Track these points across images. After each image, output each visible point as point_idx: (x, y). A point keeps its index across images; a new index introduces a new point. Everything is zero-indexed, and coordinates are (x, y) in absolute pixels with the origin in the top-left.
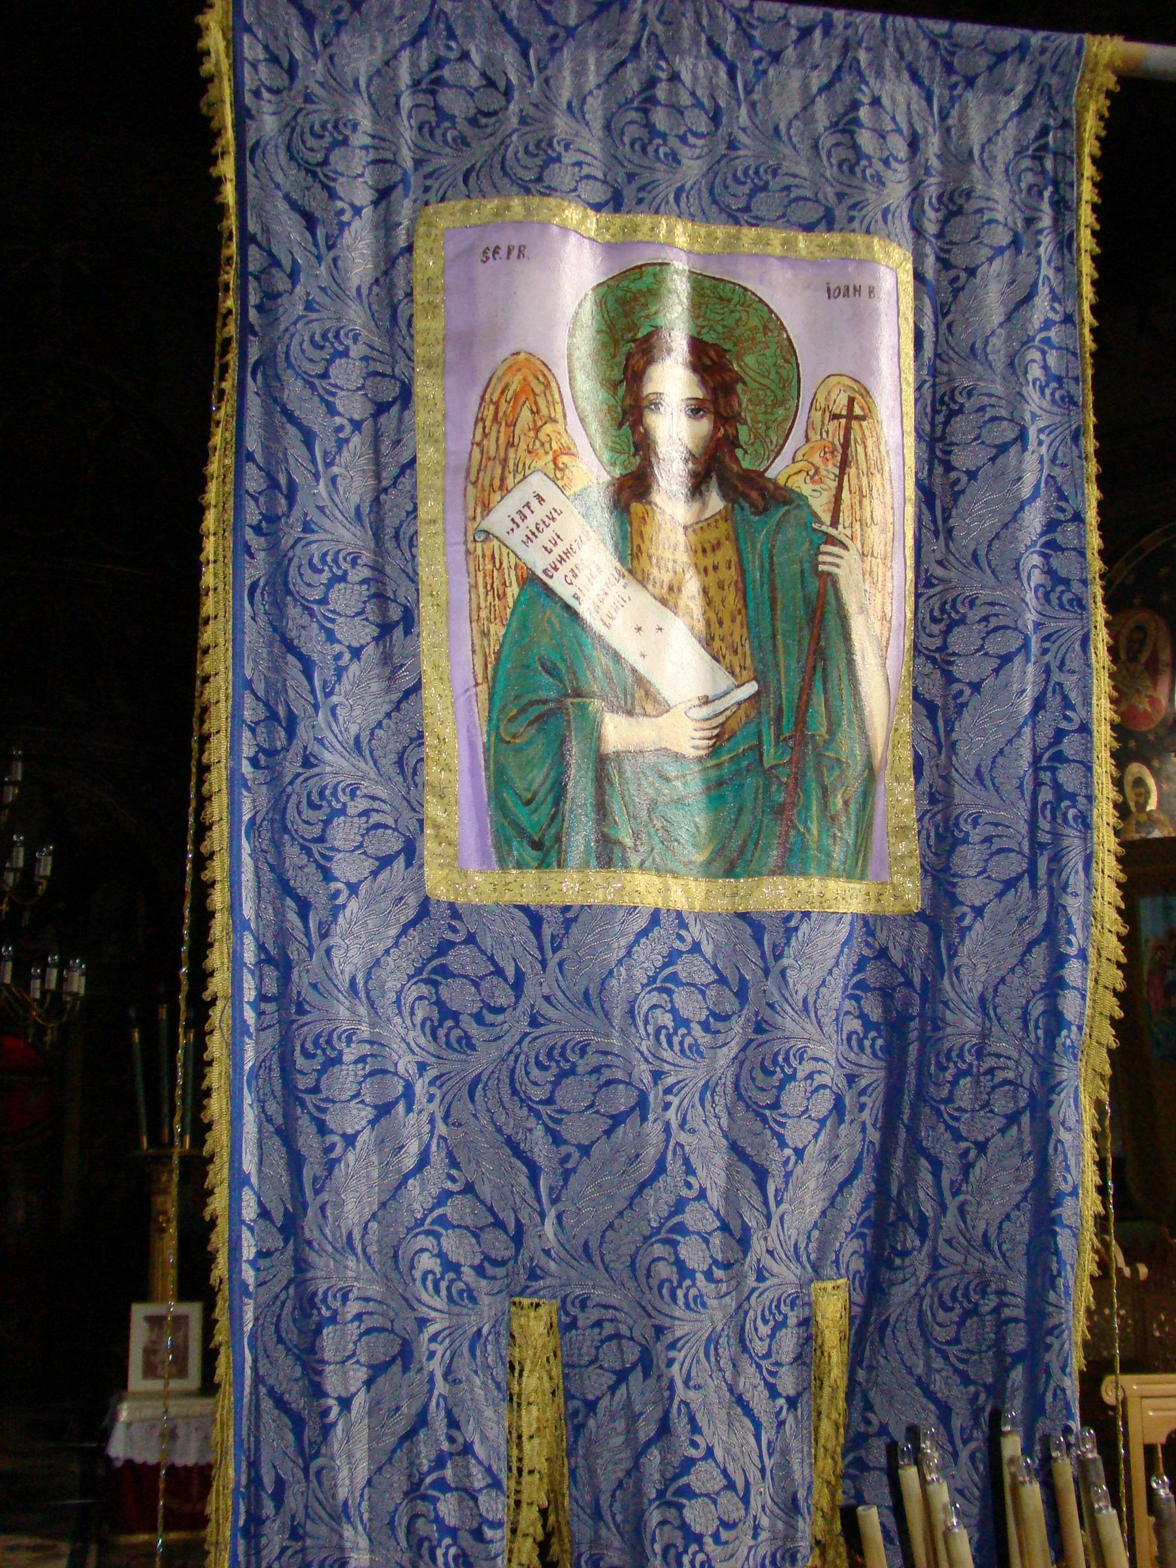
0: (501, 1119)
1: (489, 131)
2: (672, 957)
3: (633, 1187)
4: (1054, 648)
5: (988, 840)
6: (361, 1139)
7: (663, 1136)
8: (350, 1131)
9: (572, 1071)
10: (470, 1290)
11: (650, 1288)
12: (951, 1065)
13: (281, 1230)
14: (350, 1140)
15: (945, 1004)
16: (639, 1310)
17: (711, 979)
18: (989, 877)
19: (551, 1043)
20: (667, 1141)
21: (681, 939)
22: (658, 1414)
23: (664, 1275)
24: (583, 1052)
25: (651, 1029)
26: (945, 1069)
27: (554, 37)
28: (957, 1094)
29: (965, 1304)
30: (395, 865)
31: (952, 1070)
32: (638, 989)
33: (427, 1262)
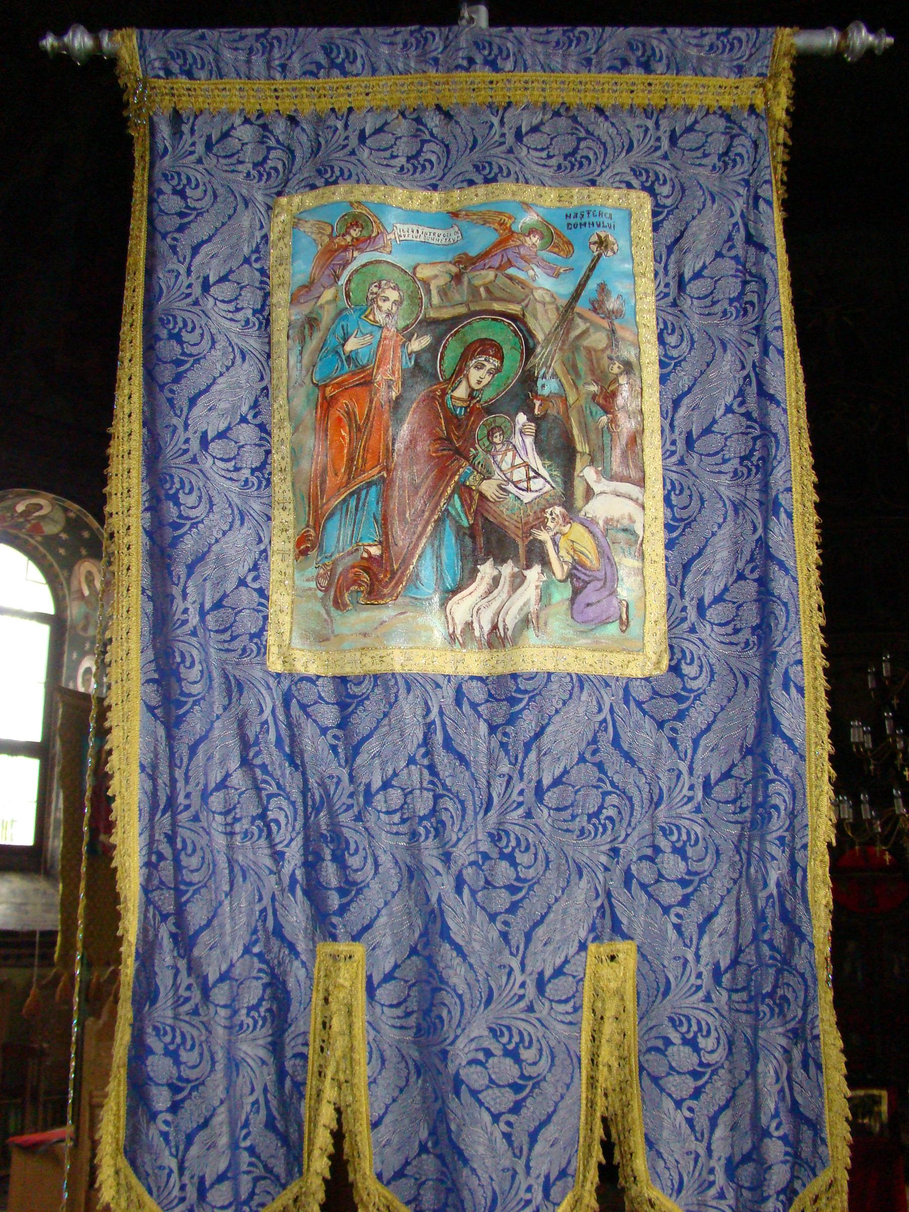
0: (612, 131)
1: (618, 178)
2: (516, 1108)
3: (547, 920)
4: (187, 146)
5: (237, 469)
6: (722, 411)
7: (527, 961)
8: (730, 416)
9: (590, 817)
10: (632, 49)
11: (538, 1040)
12: (263, 1014)
13: (780, 505)
14: (729, 410)
15: (264, 1062)
16: (545, 1023)
17: (484, 1094)
18: (233, 609)
19: (581, 171)
20: (523, 958)
21: (509, 1124)
22: (532, 947)
23: (526, 855)
24: (582, 831)
25: (532, 849)
26: (268, 1010)
27: (595, 752)
28: (250, 1185)
29: (256, 1015)
30: (691, 274)
31: (262, 1010)
32: (549, 1077)
33: (666, 190)
